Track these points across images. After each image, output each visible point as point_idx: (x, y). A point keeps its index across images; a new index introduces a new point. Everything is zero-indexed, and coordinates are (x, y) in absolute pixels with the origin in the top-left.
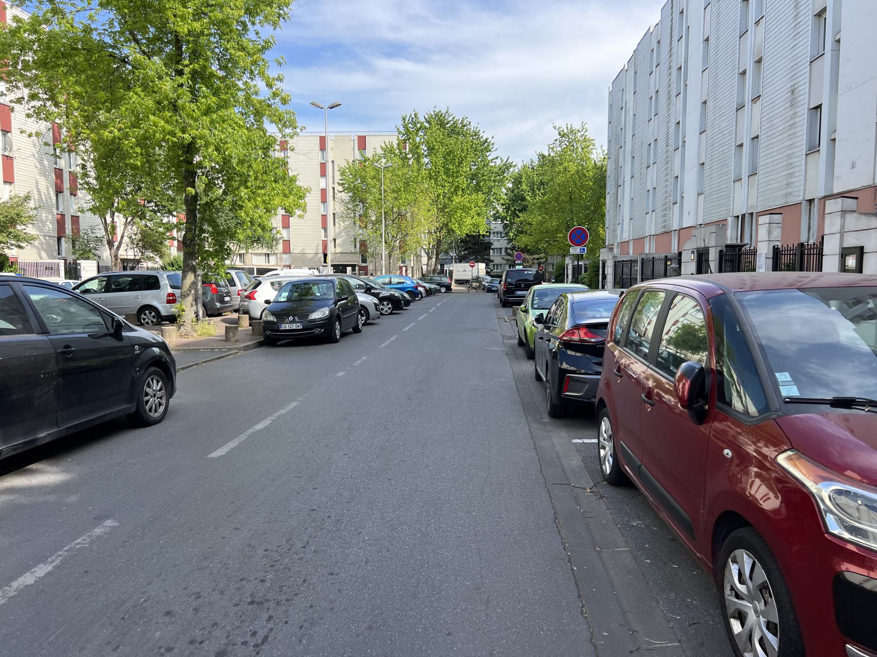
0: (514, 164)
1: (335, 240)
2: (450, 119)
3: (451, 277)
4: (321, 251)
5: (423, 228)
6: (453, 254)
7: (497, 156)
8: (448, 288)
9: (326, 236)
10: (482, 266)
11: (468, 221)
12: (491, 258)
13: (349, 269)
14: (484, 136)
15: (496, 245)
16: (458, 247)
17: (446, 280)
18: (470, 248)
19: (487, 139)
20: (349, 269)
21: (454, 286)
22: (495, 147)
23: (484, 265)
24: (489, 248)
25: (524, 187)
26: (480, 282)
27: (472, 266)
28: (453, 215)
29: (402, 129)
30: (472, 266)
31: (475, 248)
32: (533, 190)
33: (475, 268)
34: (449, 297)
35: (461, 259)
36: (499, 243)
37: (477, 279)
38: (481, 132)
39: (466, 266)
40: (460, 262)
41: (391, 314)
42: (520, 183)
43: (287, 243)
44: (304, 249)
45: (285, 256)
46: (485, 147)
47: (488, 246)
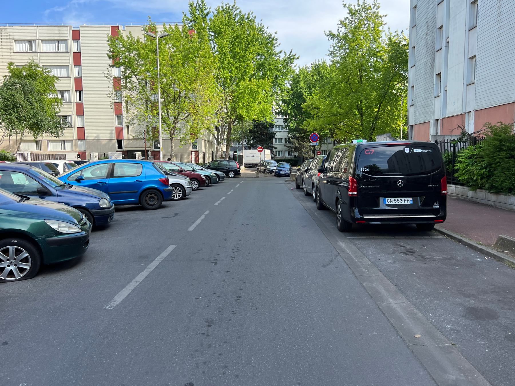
0: (296, 57)
1: (128, 127)
2: (238, 12)
3: (240, 162)
4: (114, 137)
5: (210, 104)
6: (244, 142)
7: (282, 49)
8: (237, 173)
9: (120, 123)
10: (268, 152)
11: (255, 107)
12: (274, 146)
13: (138, 155)
14: (269, 31)
15: (278, 136)
16: (248, 136)
17: (234, 165)
18: (258, 137)
19: (271, 35)
20: (138, 155)
21: (243, 170)
22: (279, 42)
23: (269, 151)
24: (273, 137)
25: (302, 84)
26: (266, 166)
27: (260, 151)
28: (240, 99)
29: (189, 16)
30: (260, 151)
31: (261, 136)
32: (310, 88)
33: (262, 153)
34: (238, 183)
35: (250, 147)
36: (281, 134)
37: (264, 164)
38: (265, 28)
39: (255, 152)
40: (250, 149)
41: (197, 189)
42: (298, 82)
43: (81, 130)
44: (98, 136)
45: (80, 143)
46: (270, 41)
47: (272, 136)
